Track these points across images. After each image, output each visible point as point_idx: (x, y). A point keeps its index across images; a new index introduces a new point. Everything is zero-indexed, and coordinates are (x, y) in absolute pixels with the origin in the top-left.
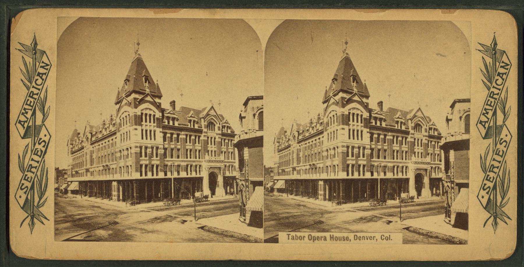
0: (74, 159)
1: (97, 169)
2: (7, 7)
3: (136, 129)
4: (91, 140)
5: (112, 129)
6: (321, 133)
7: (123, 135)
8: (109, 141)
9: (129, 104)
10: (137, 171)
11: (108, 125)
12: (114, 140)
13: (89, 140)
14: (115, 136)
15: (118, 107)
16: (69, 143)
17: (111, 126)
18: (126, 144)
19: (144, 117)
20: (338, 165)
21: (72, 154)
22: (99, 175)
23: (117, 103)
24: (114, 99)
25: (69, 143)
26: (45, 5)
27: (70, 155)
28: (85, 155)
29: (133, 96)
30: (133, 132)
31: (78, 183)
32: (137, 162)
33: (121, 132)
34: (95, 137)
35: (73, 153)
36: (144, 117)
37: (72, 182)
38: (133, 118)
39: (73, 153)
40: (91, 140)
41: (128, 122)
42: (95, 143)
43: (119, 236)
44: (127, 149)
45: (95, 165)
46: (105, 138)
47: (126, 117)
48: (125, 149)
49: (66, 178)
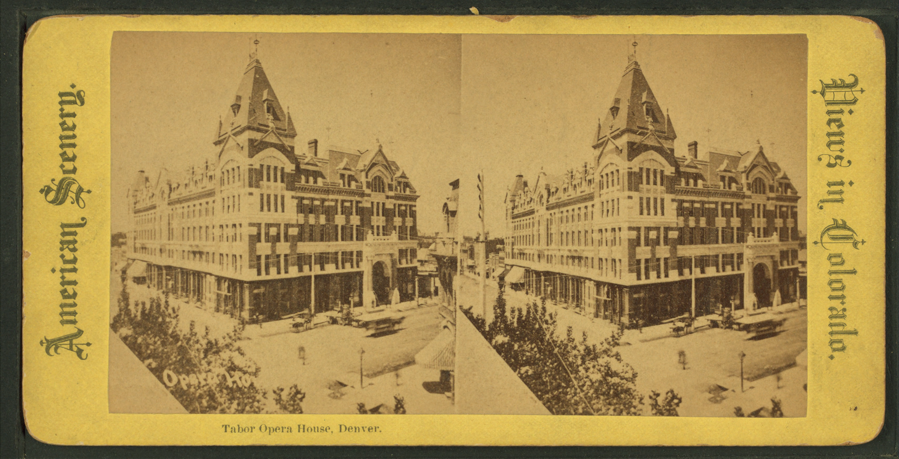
0: (515, 228)
1: (559, 254)
2: (20, 13)
3: (251, 194)
4: (548, 201)
5: (586, 189)
6: (591, 197)
7: (605, 204)
8: (573, 210)
9: (618, 151)
10: (251, 267)
11: (200, 177)
12: (590, 209)
13: (544, 200)
14: (213, 198)
15: (220, 150)
16: (508, 200)
17: (206, 180)
18: (609, 222)
19: (644, 175)
20: (620, 260)
21: (513, 218)
22: (562, 263)
23: (217, 143)
24: (591, 140)
25: (508, 200)
26: (84, 9)
27: (133, 215)
28: (536, 225)
29: (248, 135)
30: (624, 203)
31: (145, 264)
32: (632, 255)
33: (225, 195)
34: (554, 197)
35: (514, 217)
36: (644, 175)
37: (512, 266)
38: (626, 177)
39: (514, 217)
40: (548, 201)
41: (610, 183)
42: (553, 208)
43: (617, 396)
44: (601, 231)
45: (553, 246)
46: (194, 199)
47: (233, 169)
48: (609, 228)
49: (503, 259)
